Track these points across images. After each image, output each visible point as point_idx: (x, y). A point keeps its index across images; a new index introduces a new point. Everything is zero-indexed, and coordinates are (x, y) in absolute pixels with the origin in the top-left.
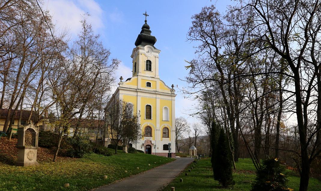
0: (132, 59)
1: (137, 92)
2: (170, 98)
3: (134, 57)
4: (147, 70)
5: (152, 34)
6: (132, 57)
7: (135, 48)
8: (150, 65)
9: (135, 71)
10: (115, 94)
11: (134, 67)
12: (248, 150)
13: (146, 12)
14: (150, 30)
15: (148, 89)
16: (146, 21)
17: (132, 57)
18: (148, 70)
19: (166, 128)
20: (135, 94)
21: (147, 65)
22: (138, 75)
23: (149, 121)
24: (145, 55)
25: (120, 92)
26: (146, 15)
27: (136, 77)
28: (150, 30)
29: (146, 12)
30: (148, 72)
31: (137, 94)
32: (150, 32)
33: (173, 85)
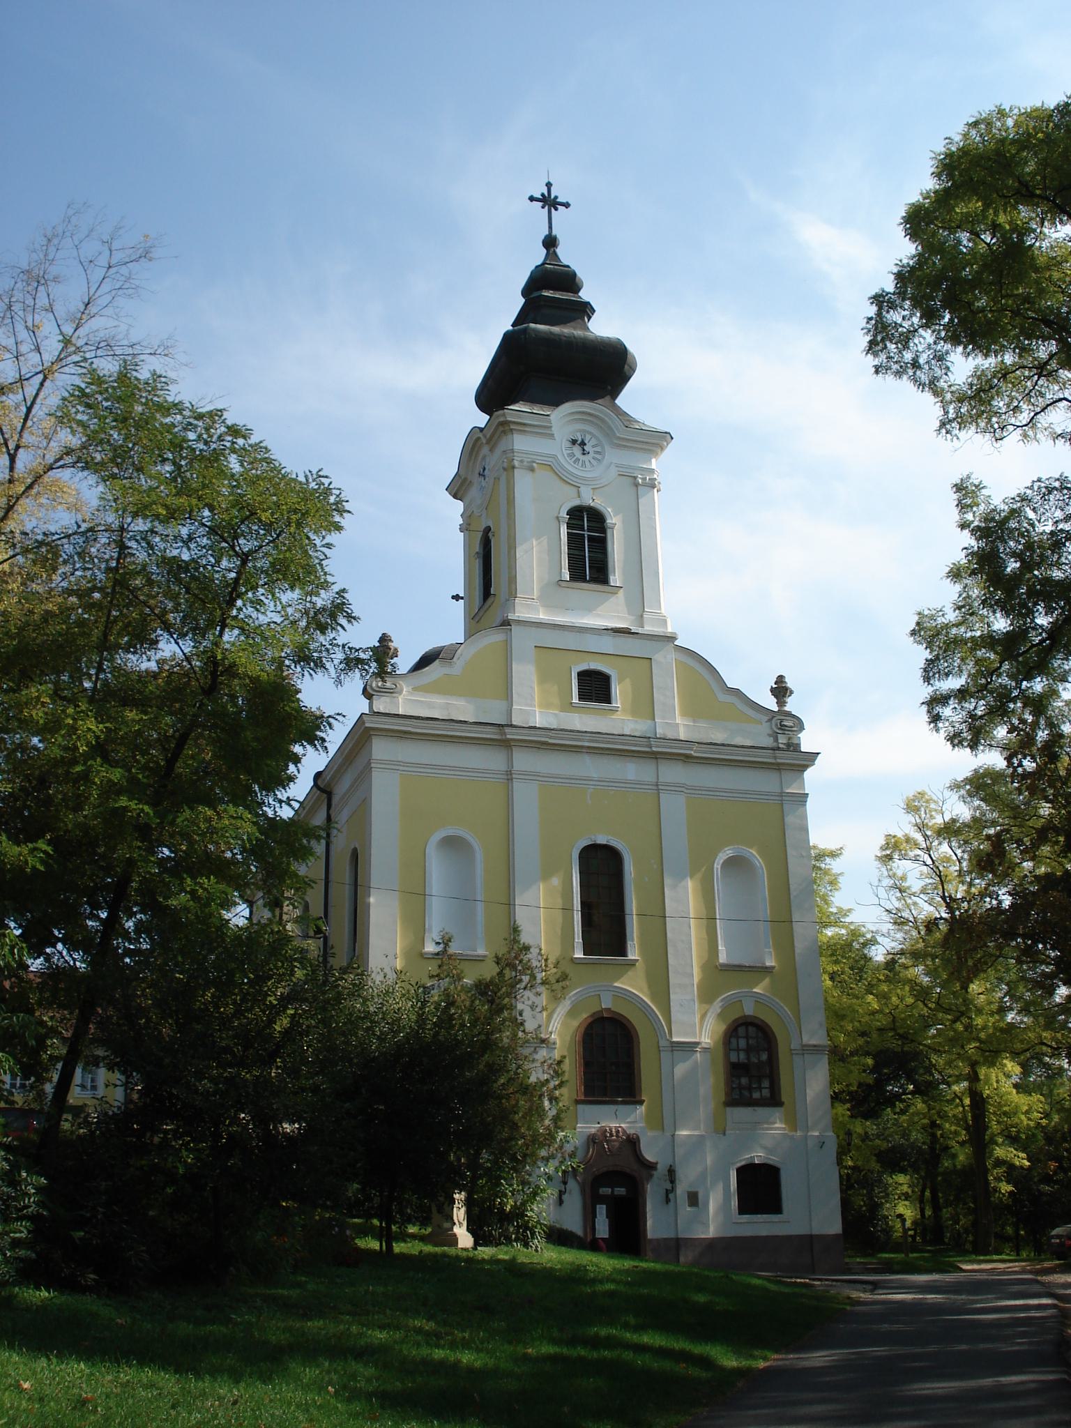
0: (459, 506)
1: (506, 744)
2: (763, 782)
3: (474, 492)
4: (577, 574)
5: (601, 327)
6: (458, 489)
7: (481, 430)
8: (600, 544)
9: (487, 593)
10: (338, 771)
11: (477, 565)
12: (774, 1010)
13: (549, 185)
14: (585, 295)
15: (588, 720)
16: (550, 243)
17: (458, 489)
18: (583, 579)
19: (752, 1024)
20: (492, 760)
21: (575, 542)
22: (506, 623)
23: (568, 971)
24: (552, 468)
25: (380, 749)
26: (549, 202)
27: (493, 638)
28: (585, 295)
29: (549, 185)
30: (587, 591)
31: (510, 760)
32: (585, 310)
33: (780, 679)
